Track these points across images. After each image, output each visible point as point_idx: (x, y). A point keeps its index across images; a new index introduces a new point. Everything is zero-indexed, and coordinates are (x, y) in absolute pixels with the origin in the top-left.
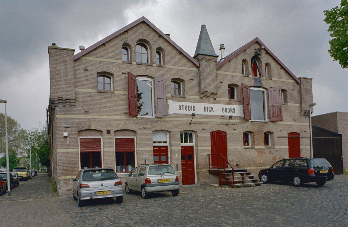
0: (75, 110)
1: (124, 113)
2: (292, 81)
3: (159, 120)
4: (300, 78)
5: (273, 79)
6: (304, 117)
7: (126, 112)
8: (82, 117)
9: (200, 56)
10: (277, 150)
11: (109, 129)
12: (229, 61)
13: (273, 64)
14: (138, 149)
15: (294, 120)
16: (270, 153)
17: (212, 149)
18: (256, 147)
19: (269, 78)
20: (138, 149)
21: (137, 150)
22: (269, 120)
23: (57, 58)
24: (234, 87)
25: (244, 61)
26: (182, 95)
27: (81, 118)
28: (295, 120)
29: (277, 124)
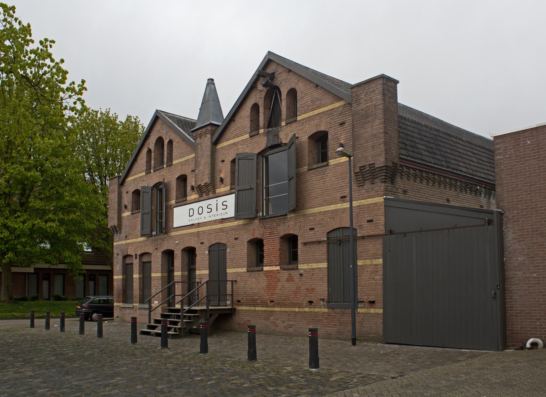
18: (265, 268)
29: (304, 215)
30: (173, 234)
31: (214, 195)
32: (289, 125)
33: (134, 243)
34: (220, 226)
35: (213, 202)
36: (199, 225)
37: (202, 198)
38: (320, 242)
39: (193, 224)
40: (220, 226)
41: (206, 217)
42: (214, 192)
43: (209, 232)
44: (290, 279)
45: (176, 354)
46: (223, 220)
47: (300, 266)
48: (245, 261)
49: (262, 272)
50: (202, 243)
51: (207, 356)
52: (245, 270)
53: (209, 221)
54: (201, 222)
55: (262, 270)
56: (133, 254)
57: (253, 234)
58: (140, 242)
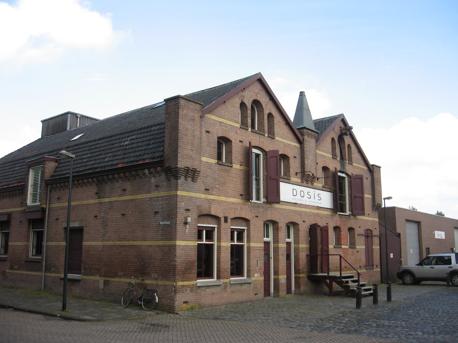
0: (196, 185)
1: (241, 195)
2: (365, 168)
3: (269, 207)
4: (373, 165)
5: (354, 164)
6: (374, 211)
7: (242, 193)
8: (203, 196)
9: (305, 131)
10: (357, 250)
11: (226, 216)
12: (225, 102)
13: (353, 146)
14: (50, 243)
15: (206, 190)
16: (353, 254)
17: (365, 249)
18: (343, 247)
19: (351, 163)
20: (50, 243)
21: (46, 246)
22: (350, 213)
23: (185, 111)
24: (223, 143)
25: (333, 139)
26: (224, 161)
27: (201, 198)
28: (208, 190)
29: (357, 219)
30: (276, 206)
31: (312, 186)
32: (241, 129)
33: (222, 202)
34: (316, 211)
35: (306, 190)
36: (301, 205)
37: (302, 184)
38: (362, 235)
39: (296, 203)
40: (316, 211)
41: (305, 201)
42: (312, 184)
43: (310, 214)
44: (353, 254)
45: (235, 317)
46: (318, 208)
47: (357, 247)
48: (179, 220)
49: (340, 249)
50: (304, 221)
51: (359, 311)
52: (347, 247)
53: (309, 205)
54: (303, 203)
55: (341, 248)
56: (221, 216)
57: (336, 223)
58: (233, 203)
